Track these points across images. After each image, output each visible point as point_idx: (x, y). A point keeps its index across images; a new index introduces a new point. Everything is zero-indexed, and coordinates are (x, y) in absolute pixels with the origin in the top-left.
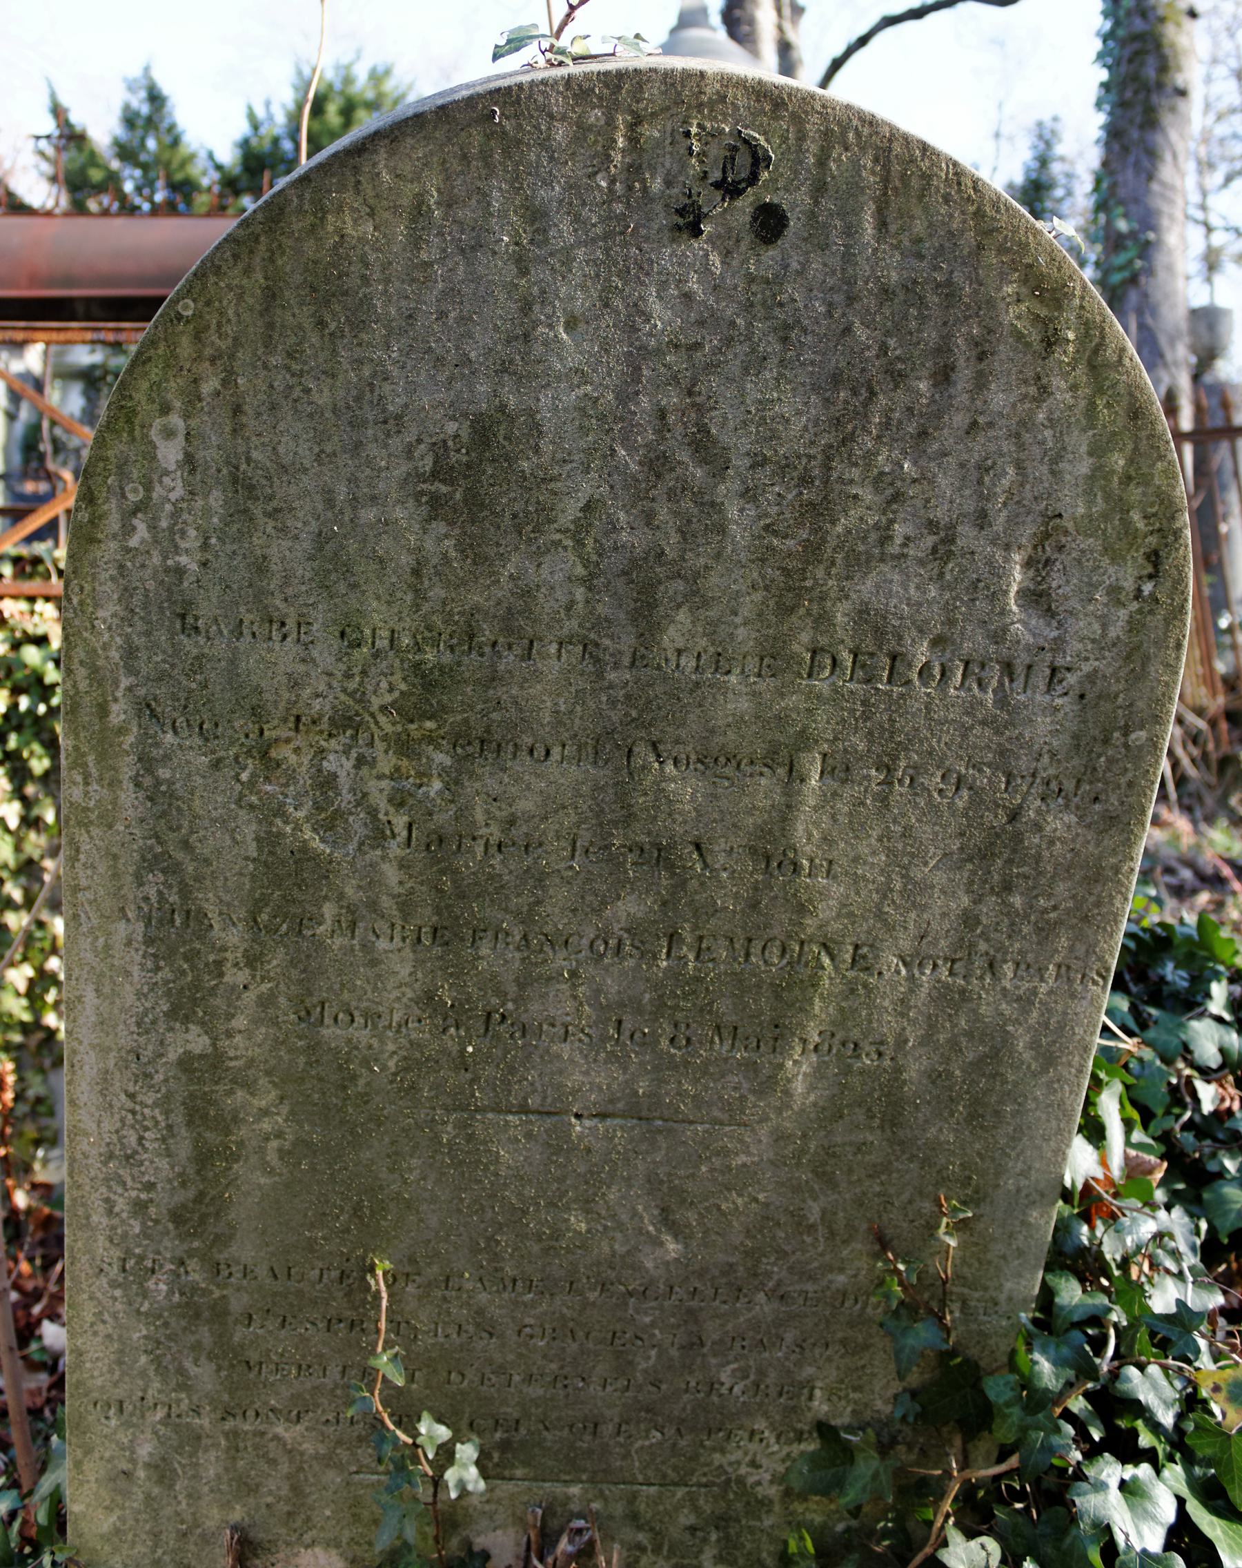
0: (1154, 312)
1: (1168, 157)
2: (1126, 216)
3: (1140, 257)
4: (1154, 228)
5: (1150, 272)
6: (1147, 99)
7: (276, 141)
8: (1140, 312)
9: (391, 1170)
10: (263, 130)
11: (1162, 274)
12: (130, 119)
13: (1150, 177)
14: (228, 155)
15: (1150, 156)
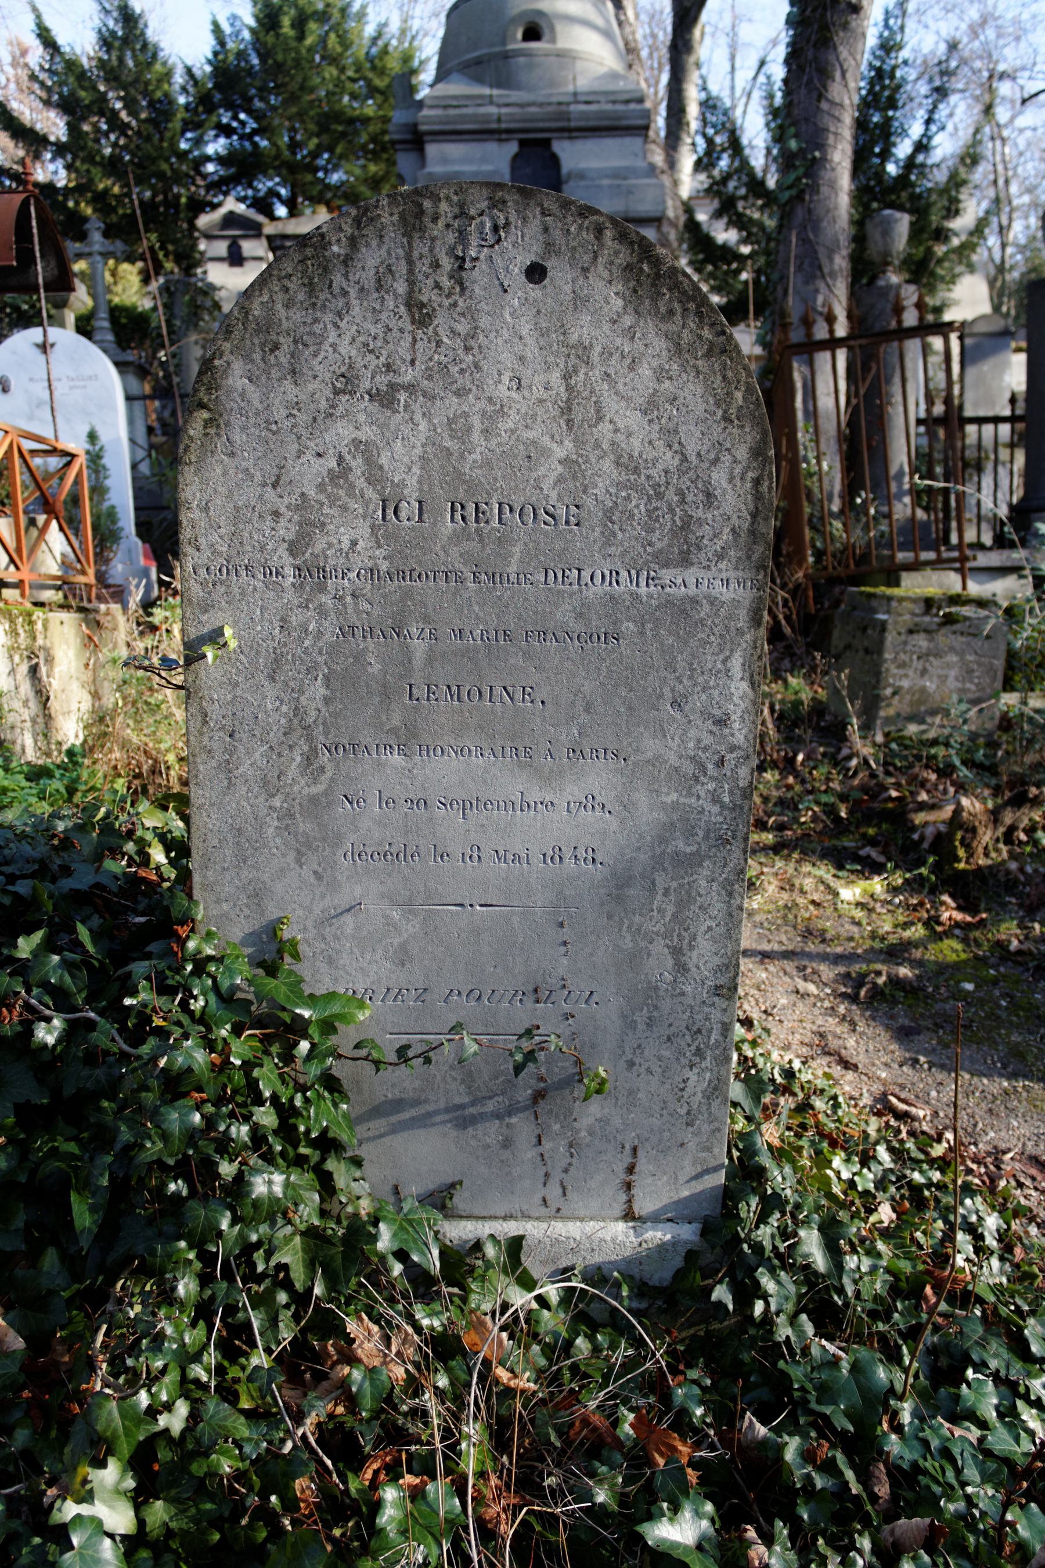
0: (816, 229)
1: (838, 75)
2: (796, 136)
3: (806, 175)
4: (822, 147)
5: (815, 188)
6: (823, 16)
7: (241, 55)
8: (804, 227)
9: (939, 1141)
10: (230, 45)
11: (824, 190)
12: (106, 41)
13: (820, 97)
14: (203, 69)
15: (824, 74)
